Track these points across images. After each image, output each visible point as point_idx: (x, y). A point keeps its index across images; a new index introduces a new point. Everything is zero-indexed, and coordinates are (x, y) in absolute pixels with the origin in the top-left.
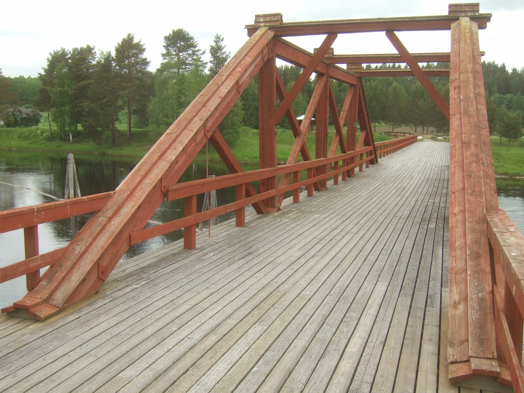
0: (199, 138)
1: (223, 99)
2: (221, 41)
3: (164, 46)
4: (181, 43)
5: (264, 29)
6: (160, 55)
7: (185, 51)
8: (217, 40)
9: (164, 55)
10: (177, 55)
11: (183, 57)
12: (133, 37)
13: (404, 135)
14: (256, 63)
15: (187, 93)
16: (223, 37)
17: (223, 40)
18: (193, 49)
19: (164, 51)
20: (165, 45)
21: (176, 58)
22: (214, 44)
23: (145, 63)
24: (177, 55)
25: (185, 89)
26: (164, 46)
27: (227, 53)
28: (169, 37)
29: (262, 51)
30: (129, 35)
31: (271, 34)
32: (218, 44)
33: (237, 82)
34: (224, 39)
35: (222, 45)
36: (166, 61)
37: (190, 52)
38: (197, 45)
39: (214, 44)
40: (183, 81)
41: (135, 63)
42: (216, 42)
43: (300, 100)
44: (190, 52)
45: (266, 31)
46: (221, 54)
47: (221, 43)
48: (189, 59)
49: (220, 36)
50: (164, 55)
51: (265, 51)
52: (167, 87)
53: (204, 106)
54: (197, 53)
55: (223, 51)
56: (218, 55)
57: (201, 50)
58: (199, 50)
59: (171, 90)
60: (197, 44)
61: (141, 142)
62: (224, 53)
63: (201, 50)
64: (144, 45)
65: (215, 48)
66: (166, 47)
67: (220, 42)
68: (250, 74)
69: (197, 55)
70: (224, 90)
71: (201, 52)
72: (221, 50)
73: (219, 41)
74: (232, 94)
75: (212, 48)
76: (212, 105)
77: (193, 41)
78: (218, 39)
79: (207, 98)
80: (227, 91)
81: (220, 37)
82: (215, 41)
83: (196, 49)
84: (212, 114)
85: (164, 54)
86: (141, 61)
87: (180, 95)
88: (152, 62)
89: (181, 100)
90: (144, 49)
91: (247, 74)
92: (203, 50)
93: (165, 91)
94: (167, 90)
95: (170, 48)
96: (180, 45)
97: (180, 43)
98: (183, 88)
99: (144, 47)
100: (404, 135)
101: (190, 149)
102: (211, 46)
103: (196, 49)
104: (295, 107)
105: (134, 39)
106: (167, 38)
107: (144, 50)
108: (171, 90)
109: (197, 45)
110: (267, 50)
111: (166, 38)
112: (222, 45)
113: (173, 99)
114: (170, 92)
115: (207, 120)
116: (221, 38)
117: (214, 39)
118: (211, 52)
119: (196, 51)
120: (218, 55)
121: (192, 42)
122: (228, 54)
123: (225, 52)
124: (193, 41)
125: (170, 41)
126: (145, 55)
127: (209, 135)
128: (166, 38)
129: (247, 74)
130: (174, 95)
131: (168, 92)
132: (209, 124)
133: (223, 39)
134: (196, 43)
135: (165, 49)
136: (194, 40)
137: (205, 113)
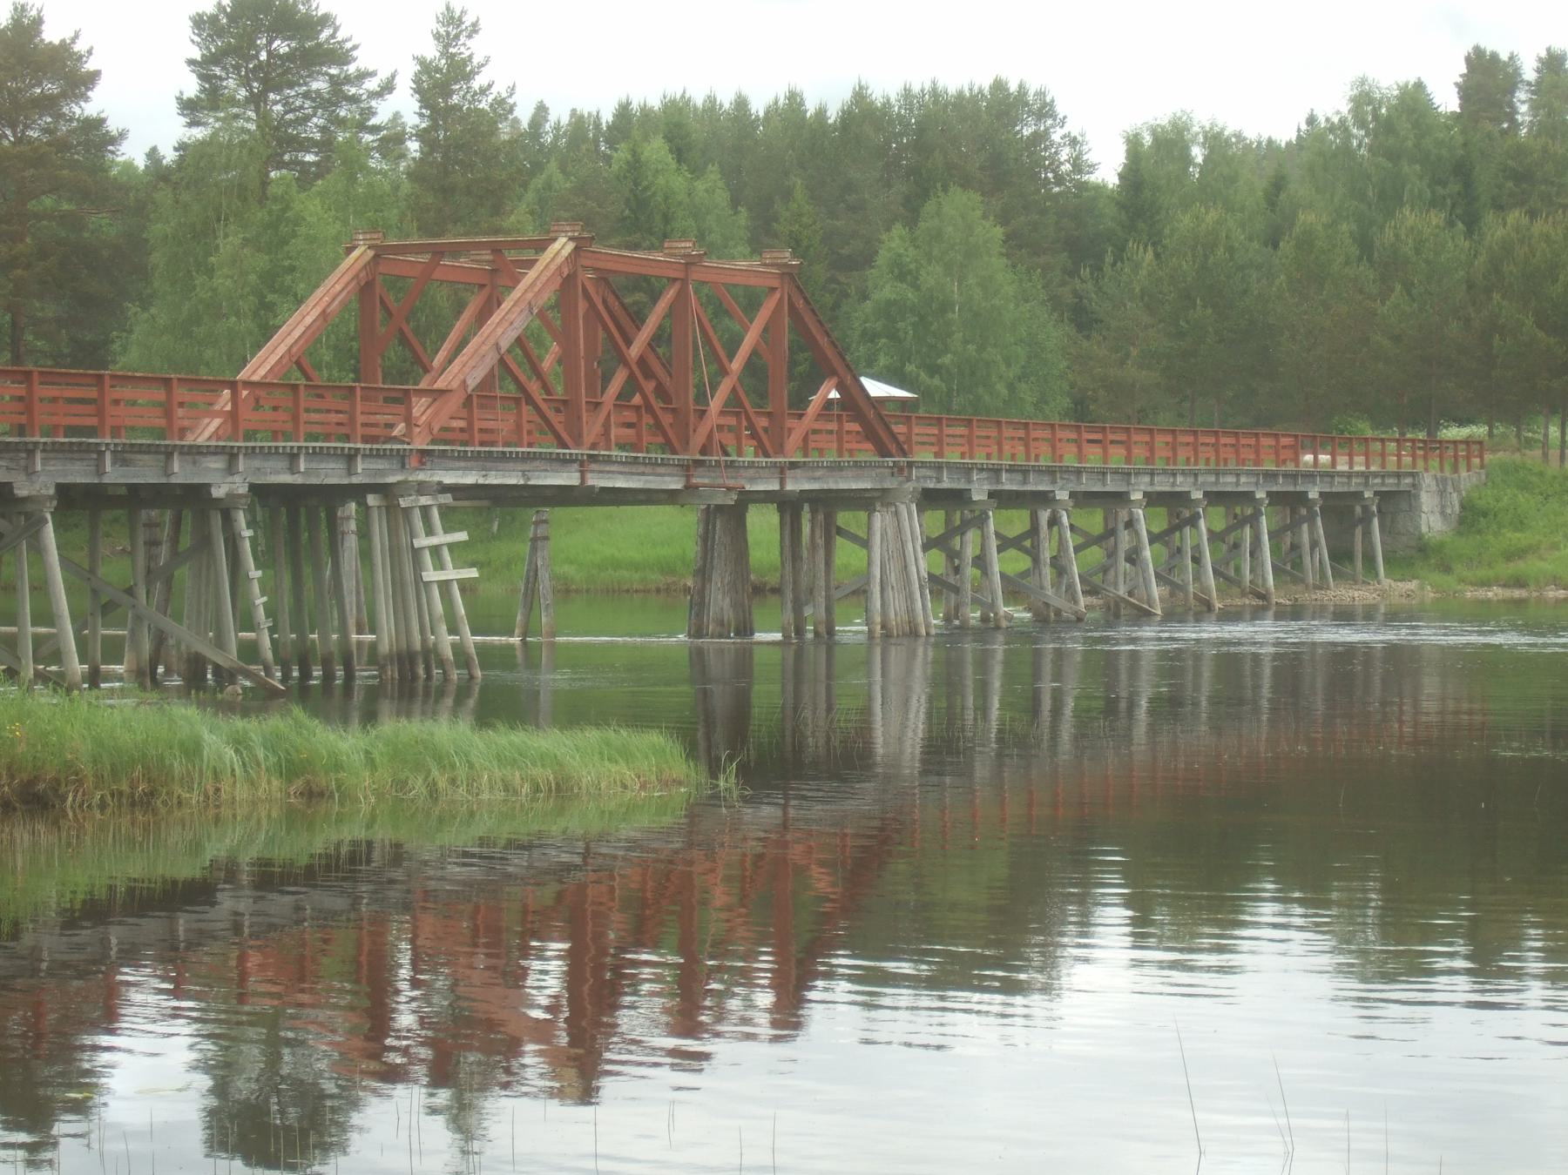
0: (284, 361)
1: (308, 328)
2: (469, 37)
3: (191, 62)
4: (275, 45)
5: (363, 248)
6: (174, 107)
7: (291, 87)
8: (448, 34)
9: (190, 108)
10: (256, 100)
11: (286, 113)
12: (38, 21)
13: (1383, 481)
14: (349, 289)
15: (302, 286)
16: (474, 20)
17: (476, 32)
18: (334, 71)
19: (191, 86)
20: (197, 54)
21: (252, 114)
22: (431, 51)
23: (96, 136)
24: (256, 100)
25: (292, 269)
26: (191, 62)
27: (500, 89)
28: (213, 19)
29: (357, 276)
30: (20, 10)
31: (371, 253)
32: (451, 50)
33: (324, 311)
34: (482, 24)
35: (470, 57)
36: (199, 133)
37: (320, 85)
38: (355, 53)
39: (431, 51)
40: (284, 229)
41: (49, 144)
42: (446, 41)
43: (996, 301)
44: (320, 85)
45: (365, 251)
46: (469, 97)
47: (469, 43)
48: (315, 120)
49: (463, 12)
50: (190, 108)
51: (363, 274)
52: (212, 259)
53: (289, 334)
54: (353, 91)
55: (476, 84)
56: (455, 99)
57: (372, 74)
58: (363, 75)
59: (228, 276)
60: (355, 47)
61: (76, 526)
62: (484, 91)
63: (372, 74)
64: (90, 52)
65: (437, 70)
66: (201, 67)
67: (462, 39)
68: (340, 302)
69: (354, 100)
70: (309, 320)
71: (372, 84)
72: (468, 77)
73: (457, 37)
74: (318, 323)
75: (426, 67)
76: (297, 333)
77: (333, 36)
78: (453, 27)
79: (292, 327)
80: (311, 320)
81: (460, 19)
82: (437, 36)
83: (352, 69)
84: (296, 341)
85: (190, 100)
86: (72, 132)
87: (270, 297)
88: (130, 135)
89: (276, 316)
90: (92, 78)
91: (336, 302)
92: (383, 75)
93: (199, 280)
94: (210, 272)
95: (217, 71)
96: (270, 53)
97: (270, 43)
98: (286, 263)
99: (90, 66)
100: (1383, 481)
101: (276, 369)
102: (422, 62)
103: (352, 69)
104: (966, 342)
105: (44, 27)
106: (204, 22)
107: (92, 78)
108: (228, 276)
109: (355, 53)
110: (364, 272)
111: (199, 22)
112: (470, 57)
113: (237, 314)
114: (223, 282)
115: (291, 346)
116: (468, 20)
117: (435, 26)
118: (418, 90)
119: (348, 80)
120: (455, 99)
121: (327, 40)
122: (504, 95)
123: (490, 86)
124: (333, 36)
125: (219, 36)
126: (94, 105)
127: (294, 360)
128: (199, 22)
129: (336, 302)
130: (241, 296)
131: (217, 281)
132: (294, 350)
133: (474, 29)
134: (348, 45)
135: (194, 76)
136: (336, 30)
137: (290, 341)
